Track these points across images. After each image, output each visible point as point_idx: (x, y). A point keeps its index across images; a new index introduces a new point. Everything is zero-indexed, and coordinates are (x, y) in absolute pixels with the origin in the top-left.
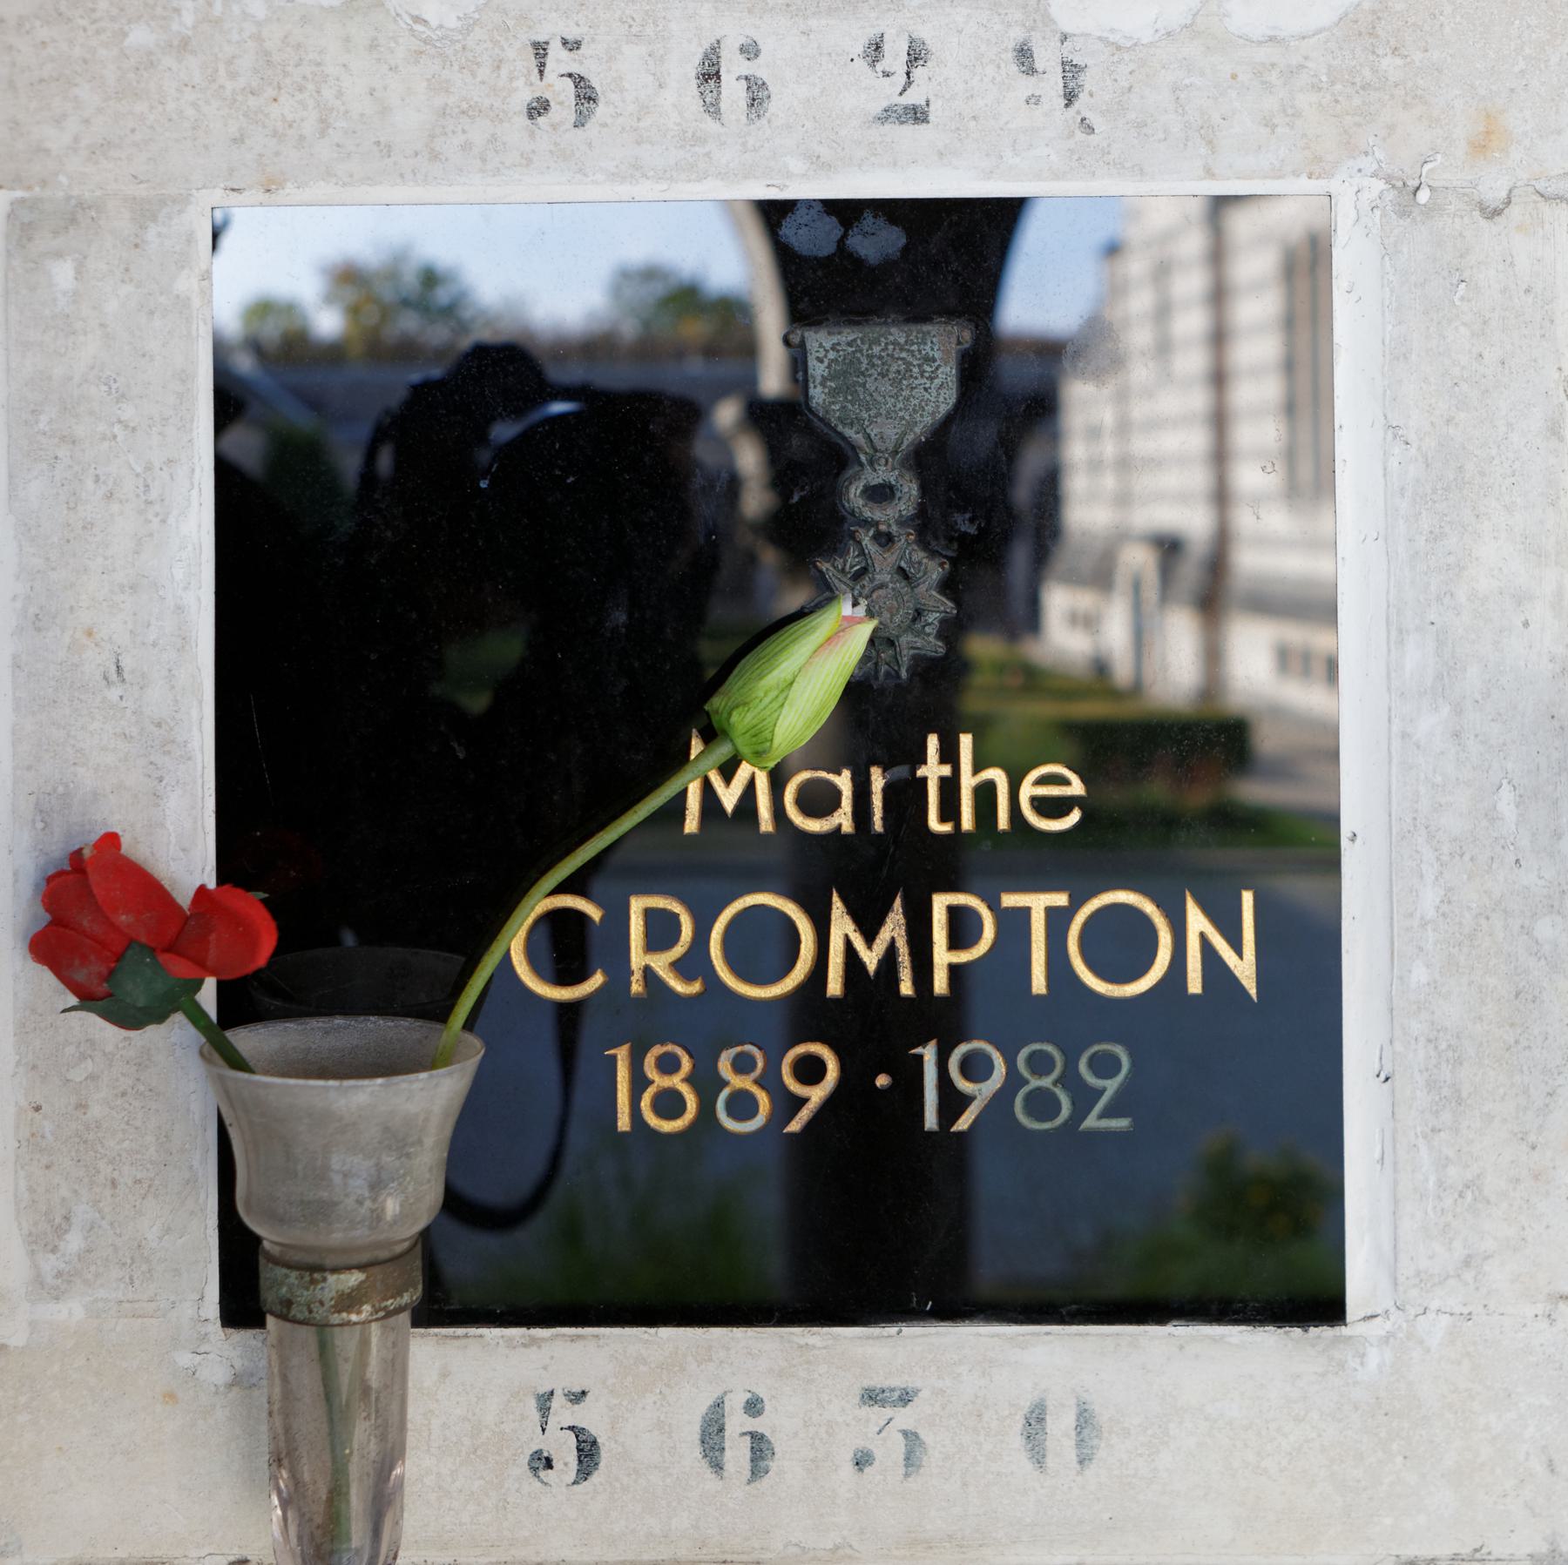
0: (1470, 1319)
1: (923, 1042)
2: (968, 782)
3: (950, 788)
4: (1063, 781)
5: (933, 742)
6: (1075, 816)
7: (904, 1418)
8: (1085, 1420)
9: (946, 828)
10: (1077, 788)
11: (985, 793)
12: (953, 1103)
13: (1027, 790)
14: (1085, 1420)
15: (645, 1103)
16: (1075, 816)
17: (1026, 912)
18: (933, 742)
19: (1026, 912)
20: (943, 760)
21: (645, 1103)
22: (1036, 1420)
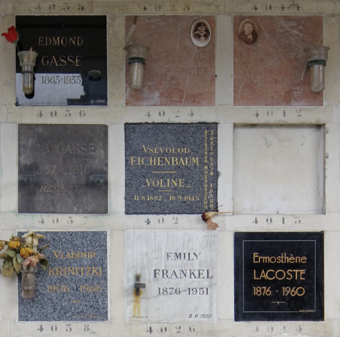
0: (190, 329)
1: (283, 287)
2: (285, 258)
3: (284, 259)
4: (304, 258)
5: (282, 254)
6: (306, 261)
7: (70, 326)
8: (162, 331)
9: (283, 262)
10: (306, 259)
11: (286, 259)
12: (286, 293)
13: (302, 259)
14: (162, 331)
15: (286, 289)
16: (306, 261)
17: (295, 272)
18: (282, 254)
19: (295, 272)
20: (283, 256)
21: (286, 289)
22: (56, 329)
